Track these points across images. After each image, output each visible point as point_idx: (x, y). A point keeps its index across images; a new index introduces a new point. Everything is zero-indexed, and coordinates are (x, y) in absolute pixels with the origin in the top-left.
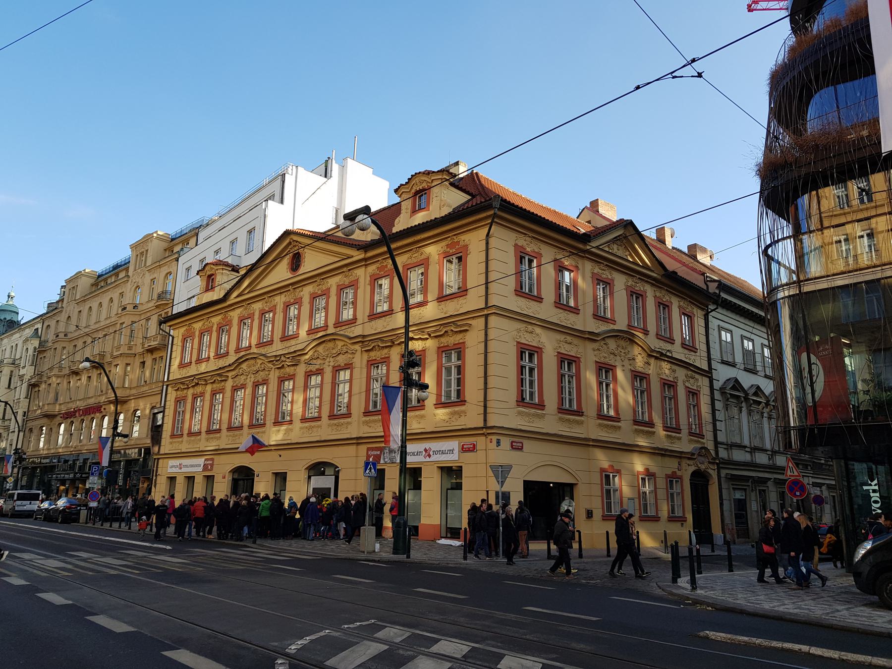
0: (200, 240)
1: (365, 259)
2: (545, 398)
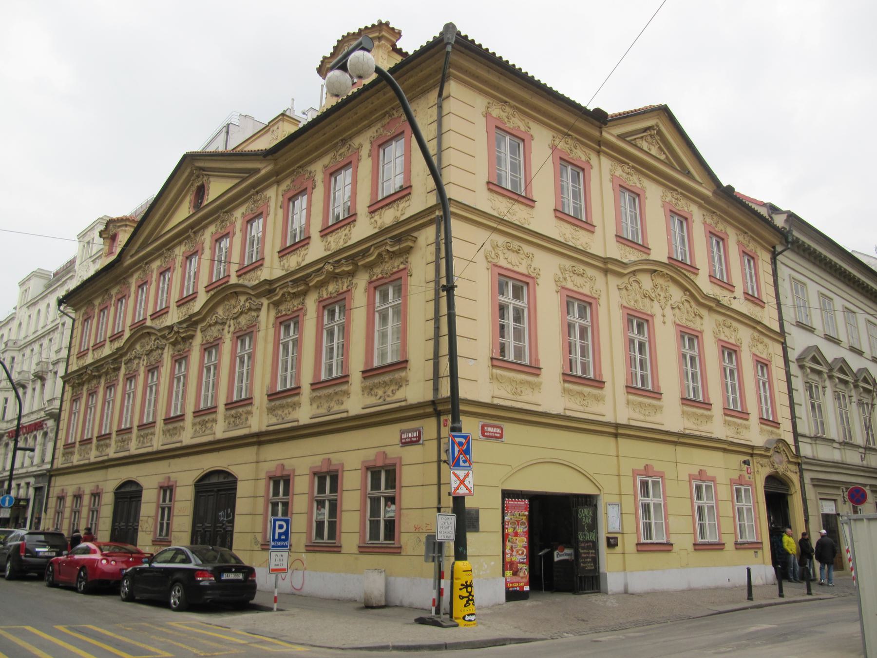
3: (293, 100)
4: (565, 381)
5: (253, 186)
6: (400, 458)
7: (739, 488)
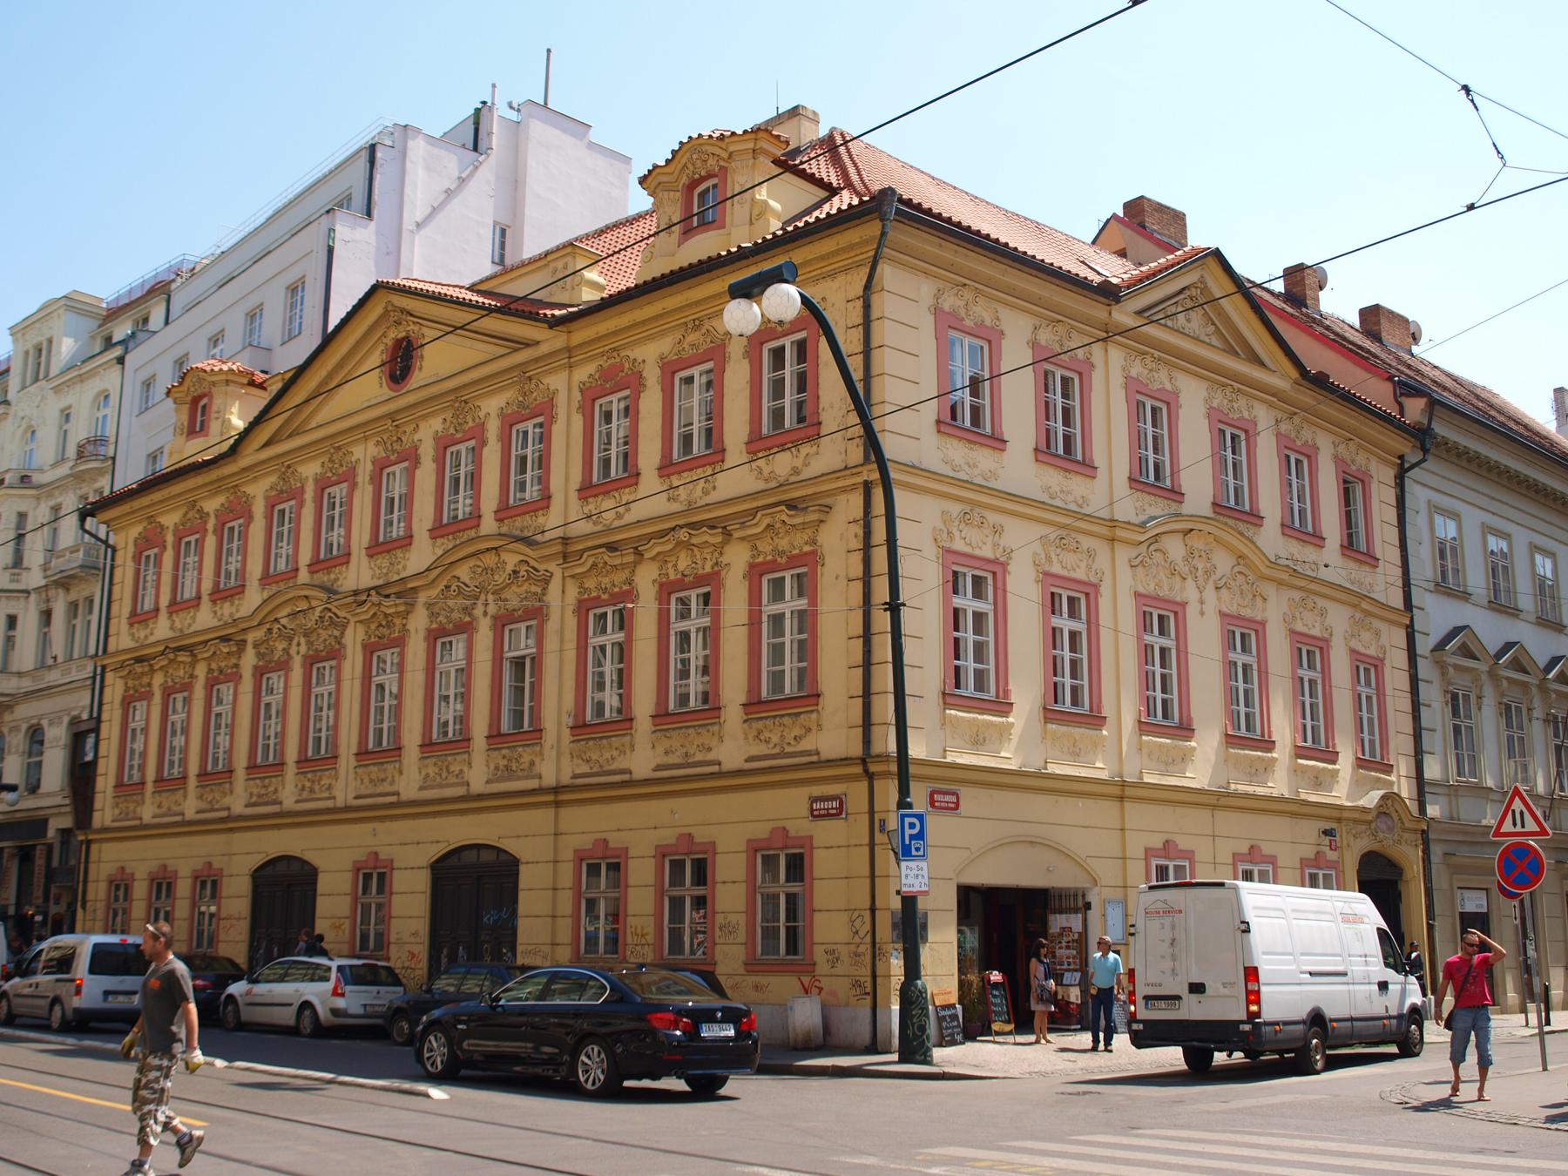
0: (176, 309)
1: (569, 350)
3: (494, 86)
4: (1047, 720)
6: (811, 838)
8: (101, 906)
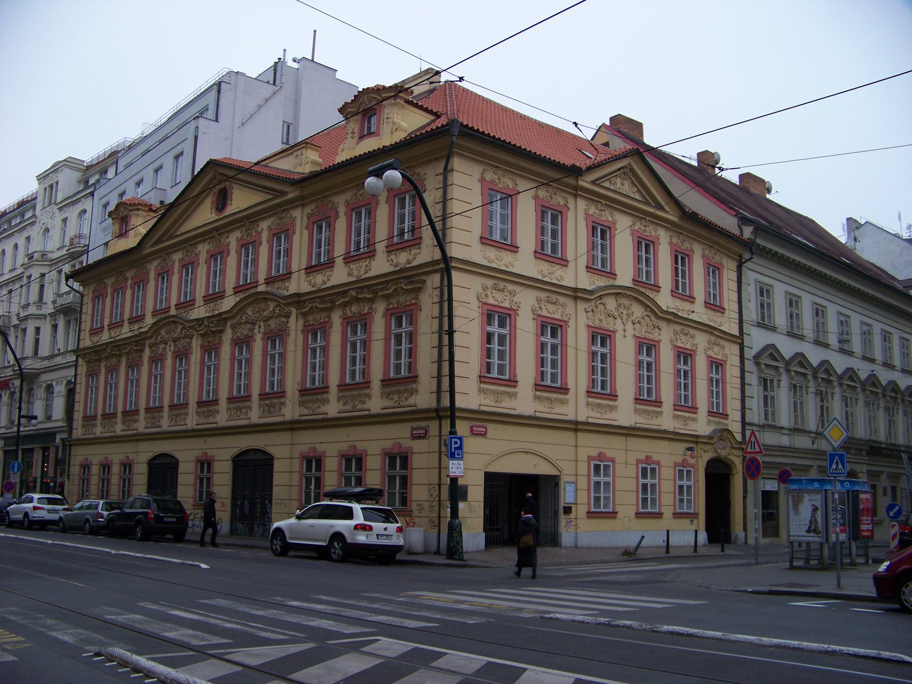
2: (518, 372)
3: (285, 50)
4: (536, 390)
5: (280, 205)
6: (411, 448)
7: (683, 470)
8: (76, 477)
